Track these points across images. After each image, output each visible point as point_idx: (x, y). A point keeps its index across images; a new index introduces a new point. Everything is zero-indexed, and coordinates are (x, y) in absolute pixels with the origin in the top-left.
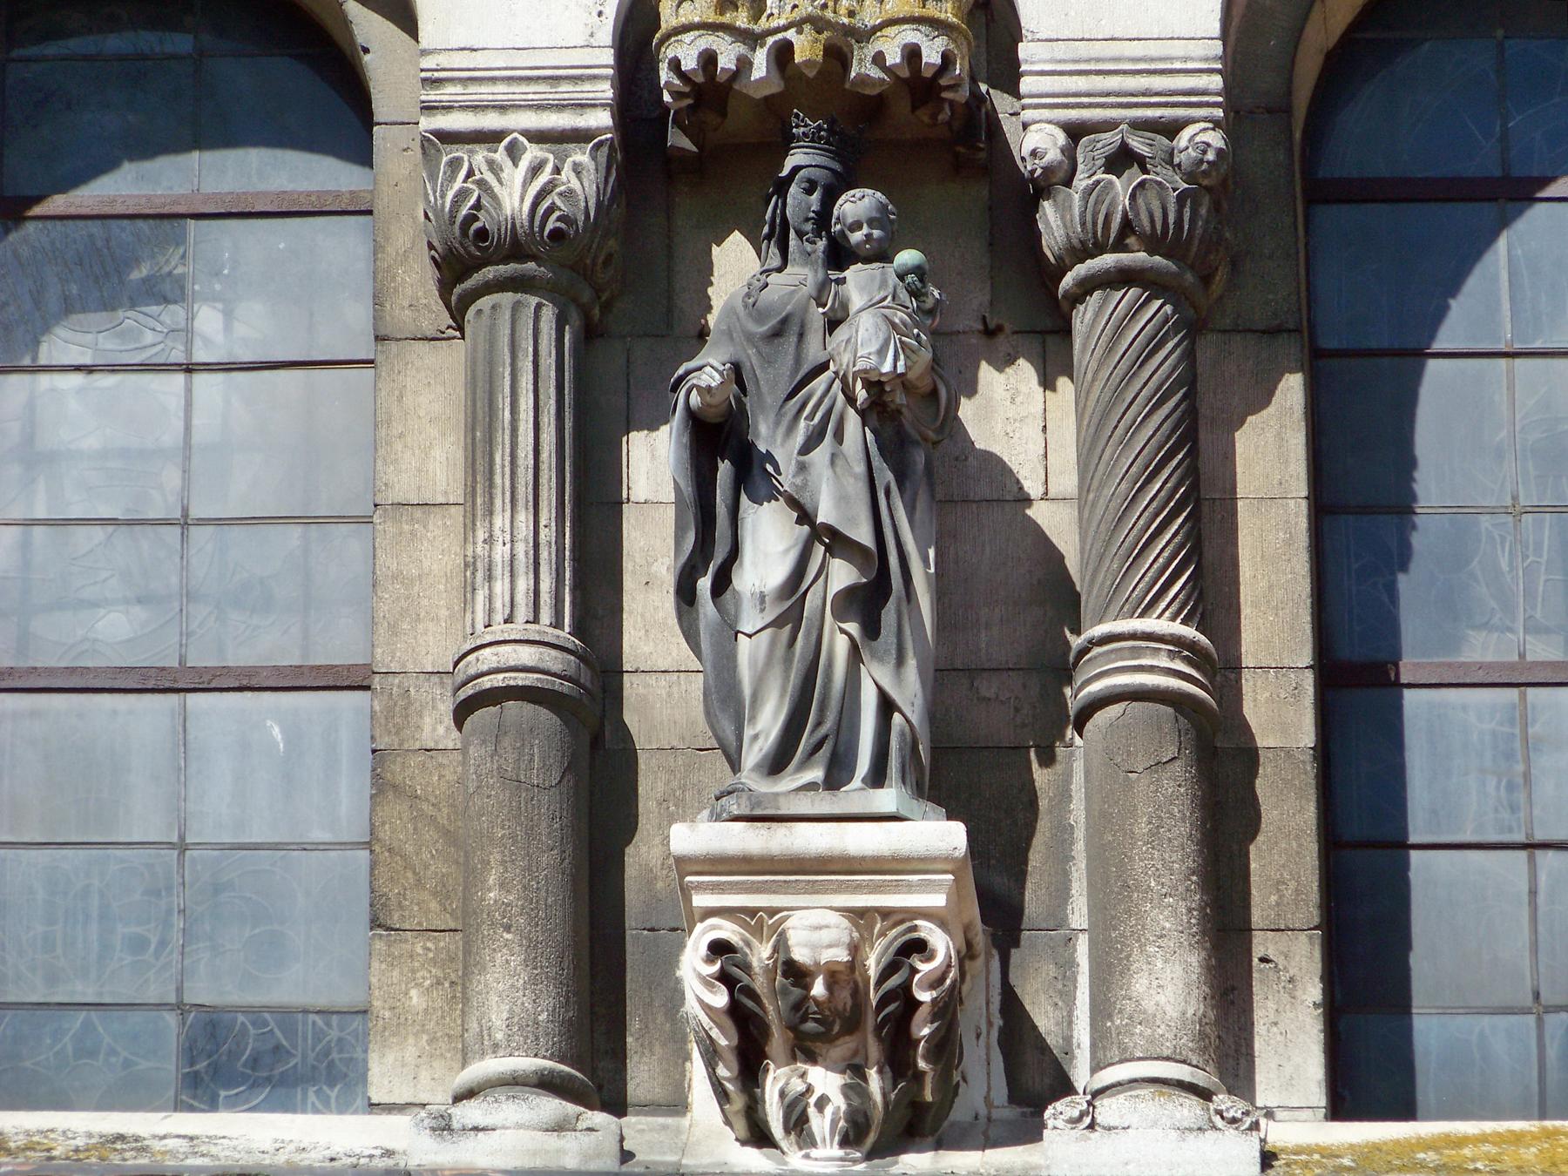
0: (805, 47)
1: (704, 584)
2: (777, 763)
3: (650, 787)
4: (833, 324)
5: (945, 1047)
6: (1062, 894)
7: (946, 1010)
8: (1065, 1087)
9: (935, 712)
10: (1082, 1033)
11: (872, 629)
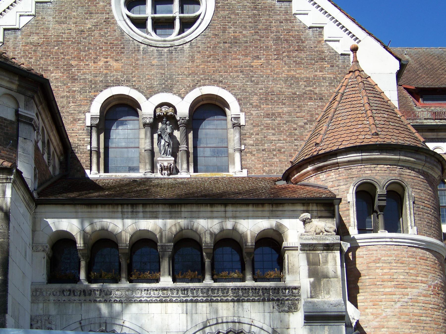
0: (165, 113)
1: (159, 144)
2: (163, 154)
3: (155, 155)
4: (167, 129)
5: (173, 170)
6: (179, 161)
7: (173, 168)
8: (179, 172)
9: (172, 151)
10: (180, 168)
11: (169, 147)
